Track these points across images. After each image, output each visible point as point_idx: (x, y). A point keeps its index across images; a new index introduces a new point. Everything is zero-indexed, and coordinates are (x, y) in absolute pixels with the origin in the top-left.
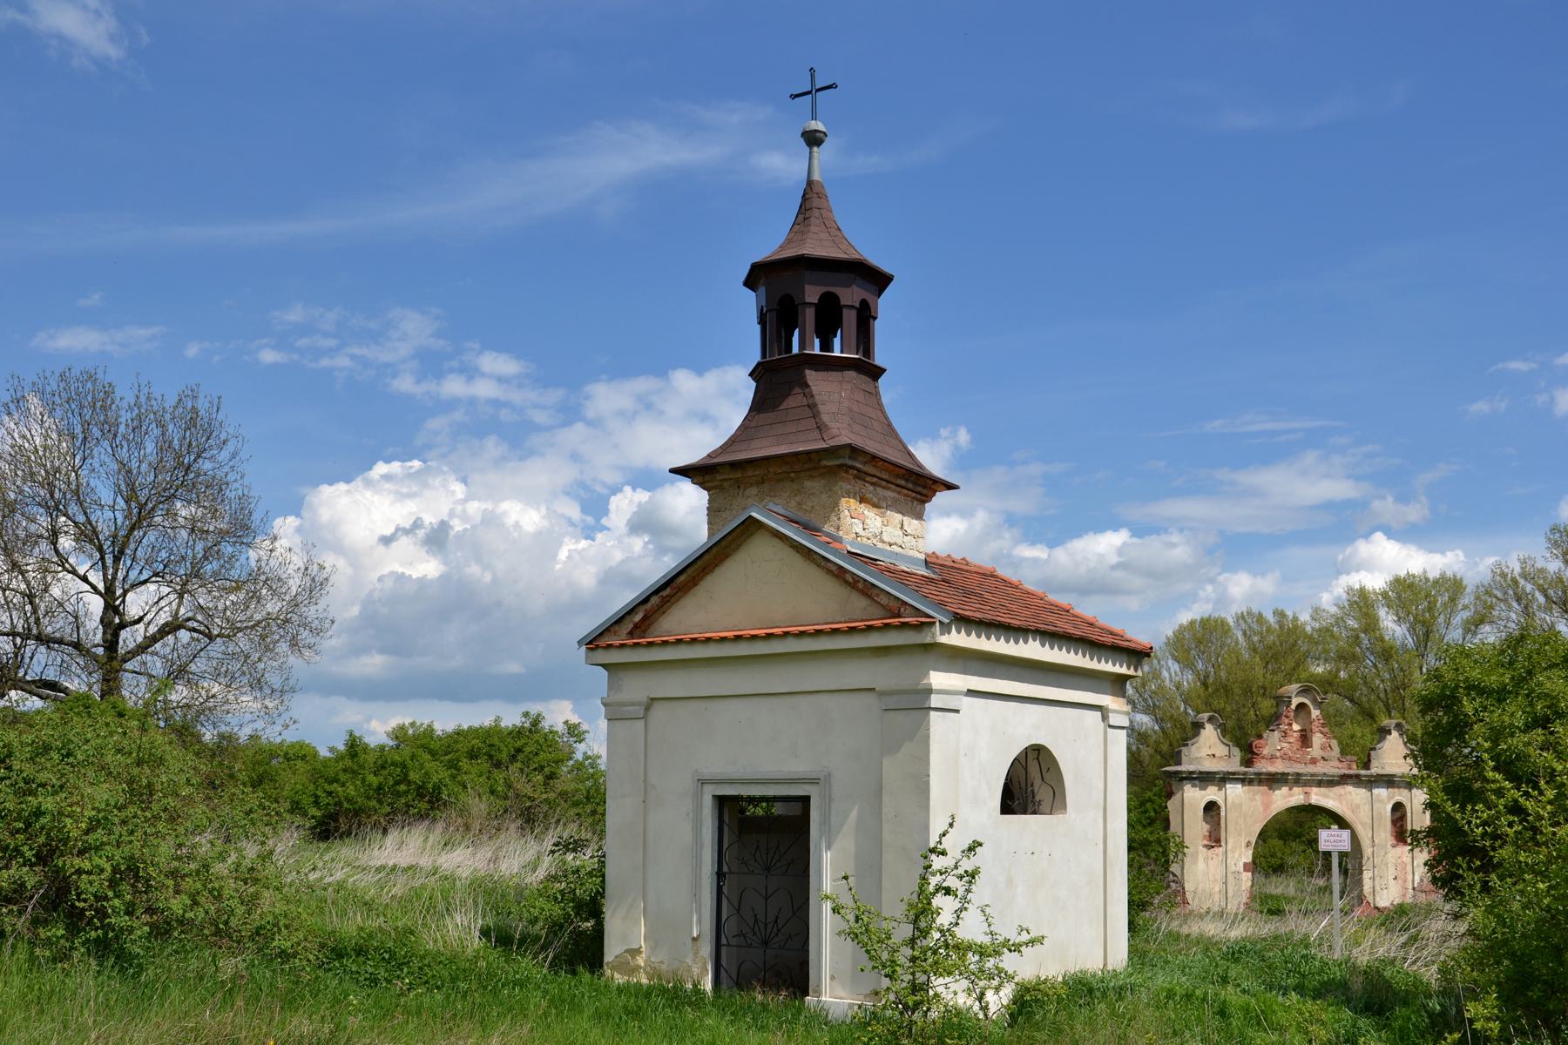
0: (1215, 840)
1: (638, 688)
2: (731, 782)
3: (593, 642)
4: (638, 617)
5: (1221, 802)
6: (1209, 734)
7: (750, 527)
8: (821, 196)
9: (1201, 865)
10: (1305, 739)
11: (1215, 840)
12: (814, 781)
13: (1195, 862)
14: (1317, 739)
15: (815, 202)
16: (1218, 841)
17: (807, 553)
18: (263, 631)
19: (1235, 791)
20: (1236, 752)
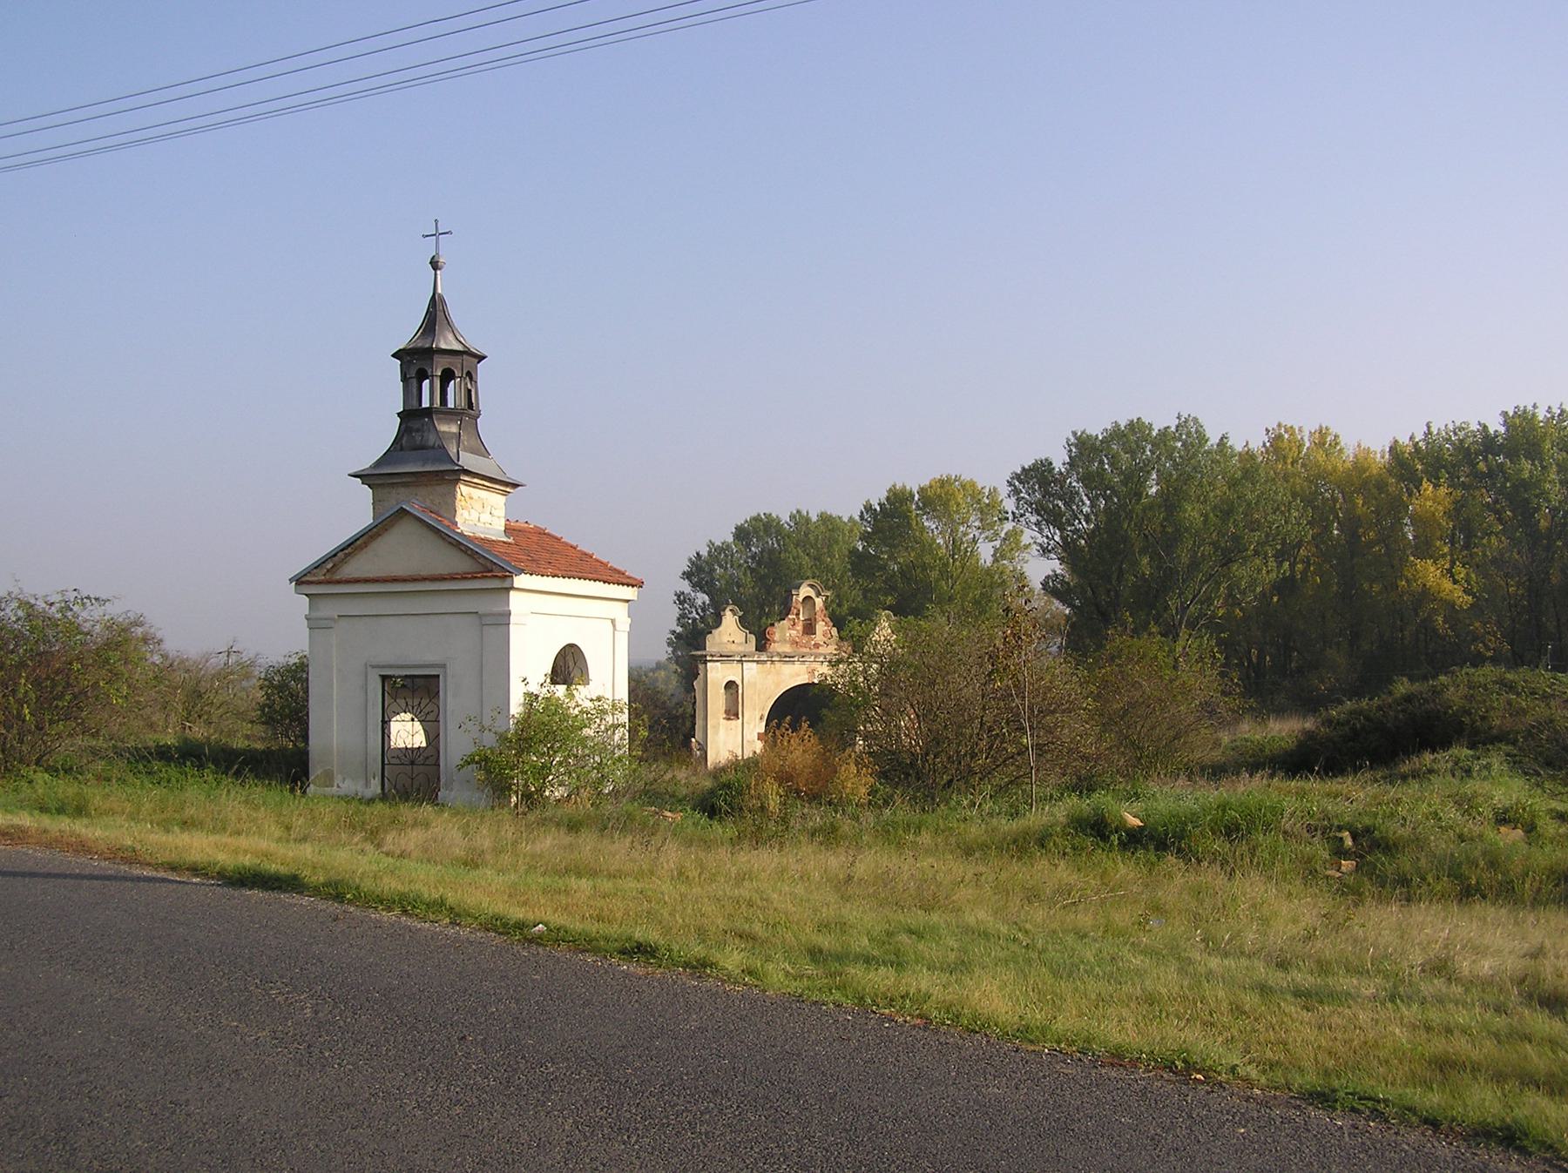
0: (732, 712)
1: (329, 609)
2: (391, 667)
3: (300, 581)
4: (330, 566)
5: (739, 682)
6: (730, 620)
7: (402, 513)
8: (443, 301)
9: (722, 731)
10: (809, 629)
11: (732, 712)
12: (444, 666)
13: (717, 733)
14: (821, 627)
15: (440, 314)
16: (737, 715)
17: (437, 531)
18: (271, 686)
19: (751, 669)
20: (752, 638)
